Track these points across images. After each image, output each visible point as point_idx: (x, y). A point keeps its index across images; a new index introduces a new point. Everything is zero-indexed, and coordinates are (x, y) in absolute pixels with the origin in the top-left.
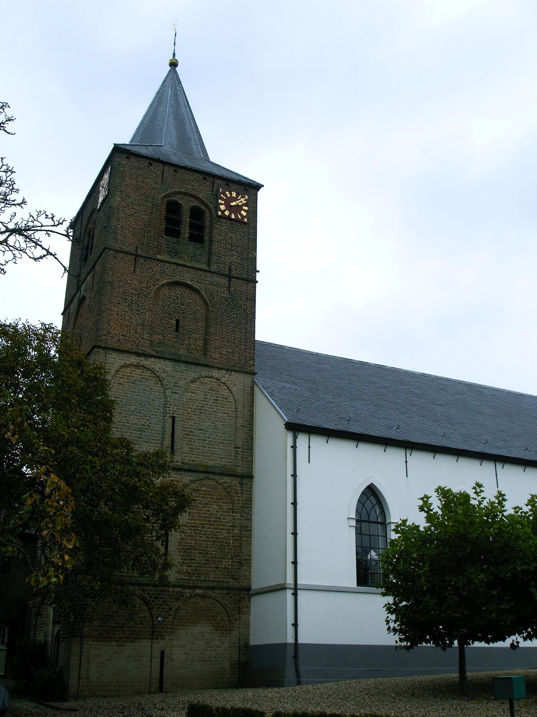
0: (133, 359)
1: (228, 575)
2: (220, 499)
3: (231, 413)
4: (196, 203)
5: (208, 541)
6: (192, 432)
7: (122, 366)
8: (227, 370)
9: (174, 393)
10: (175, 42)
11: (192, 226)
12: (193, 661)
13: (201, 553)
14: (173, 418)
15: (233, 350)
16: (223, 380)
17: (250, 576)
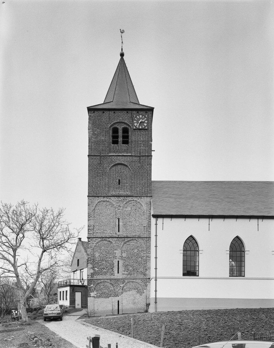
0: (102, 199)
1: (142, 274)
2: (138, 247)
3: (141, 213)
4: (125, 126)
5: (134, 262)
6: (126, 223)
7: (98, 202)
8: (139, 197)
9: (119, 209)
10: (122, 49)
11: (124, 137)
12: (129, 303)
13: (132, 267)
14: (119, 219)
15: (142, 188)
16: (138, 201)
17: (150, 274)
